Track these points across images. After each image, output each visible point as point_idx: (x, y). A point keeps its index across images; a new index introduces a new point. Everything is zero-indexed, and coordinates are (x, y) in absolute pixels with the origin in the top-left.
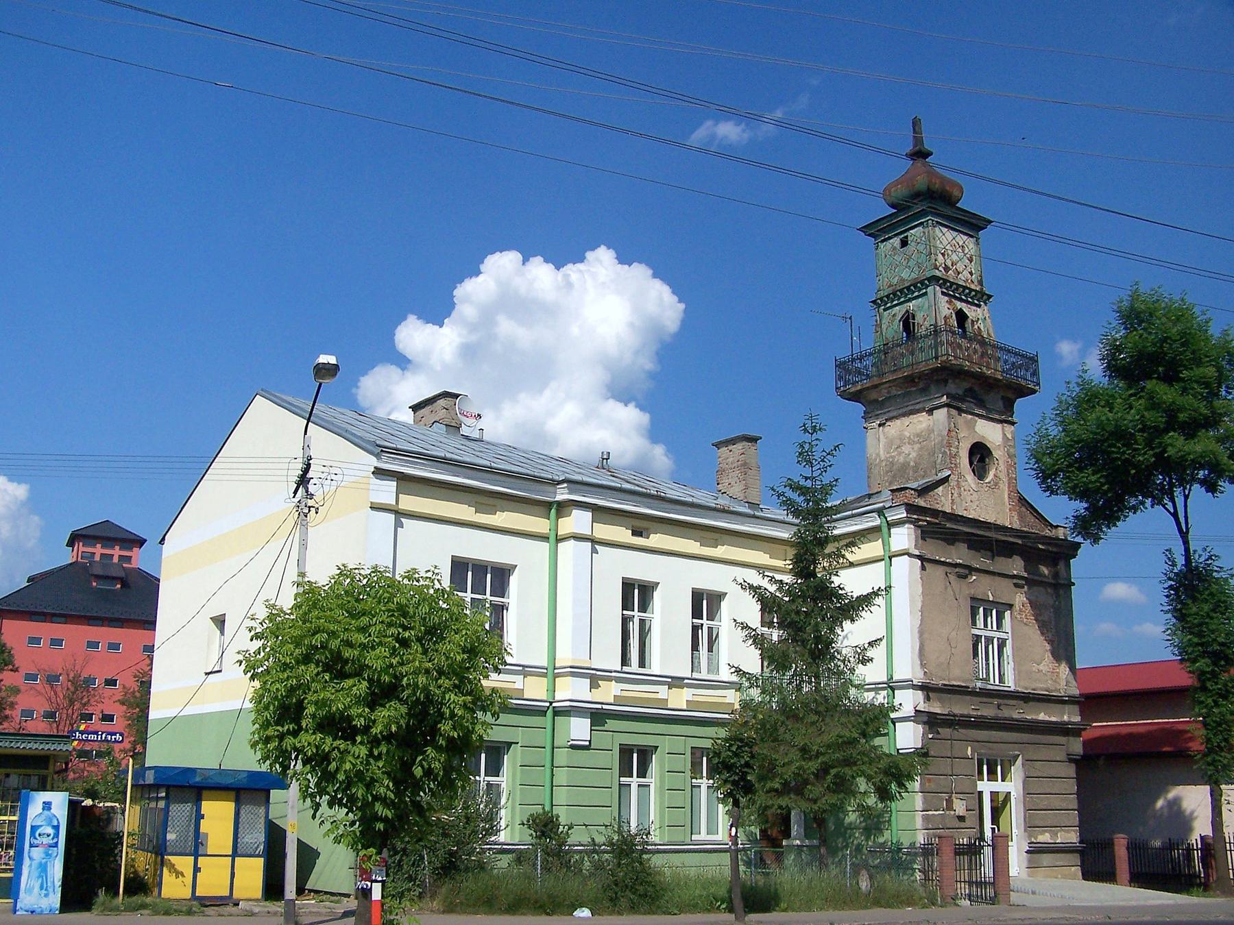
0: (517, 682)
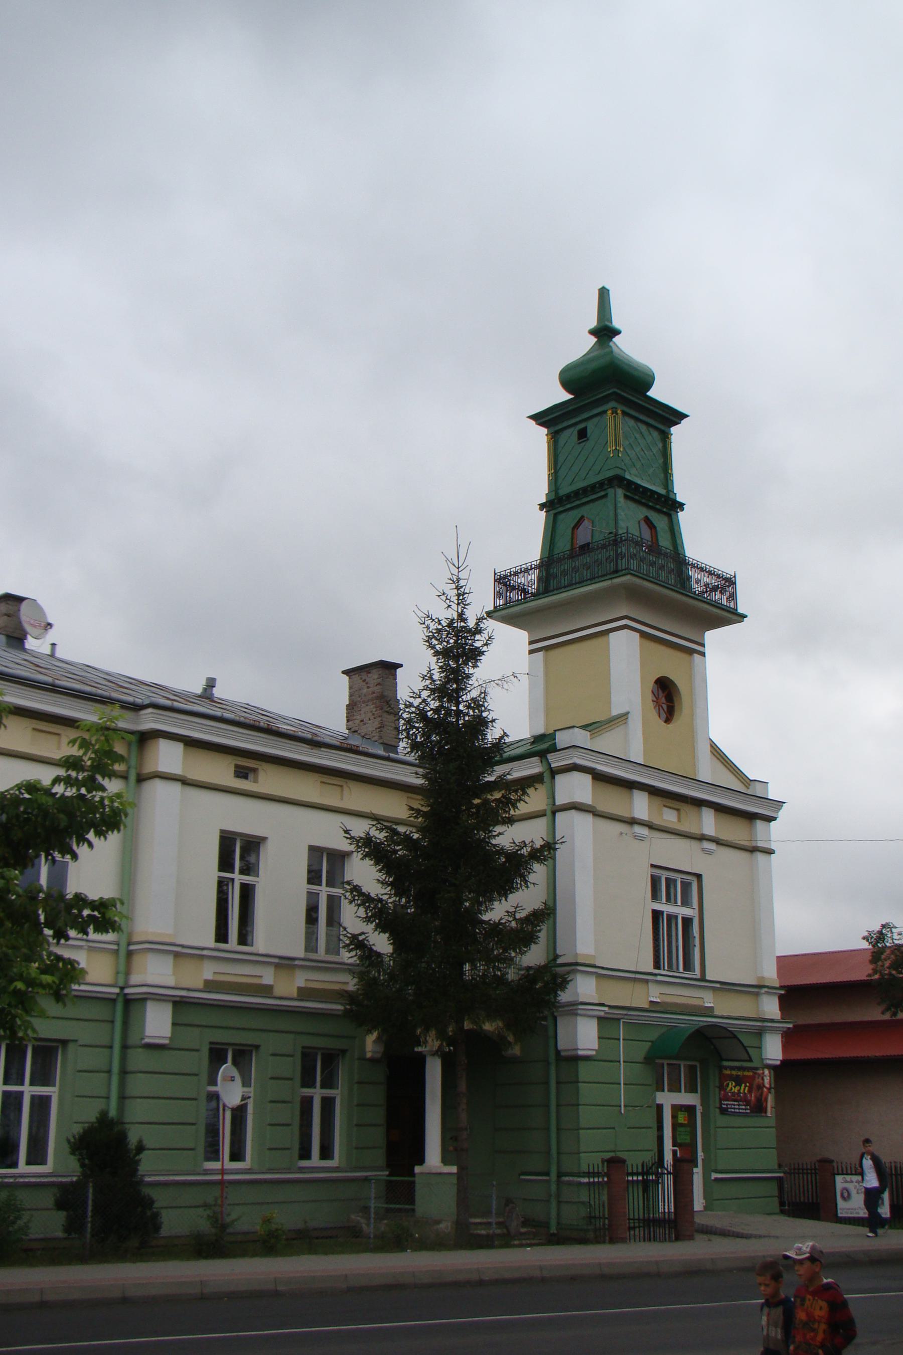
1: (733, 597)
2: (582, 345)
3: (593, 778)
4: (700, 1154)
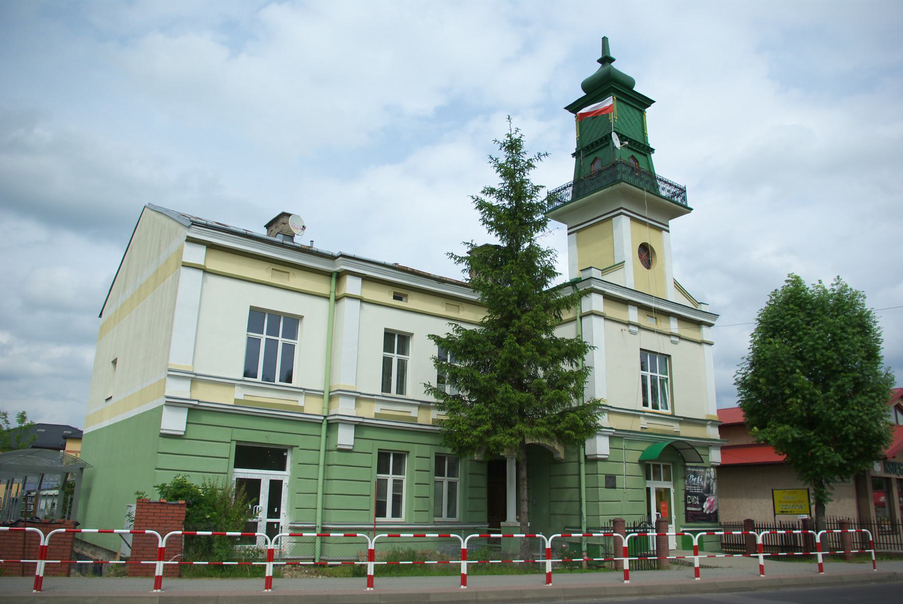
0: (301, 401)
1: (684, 199)
2: (593, 68)
4: (673, 516)
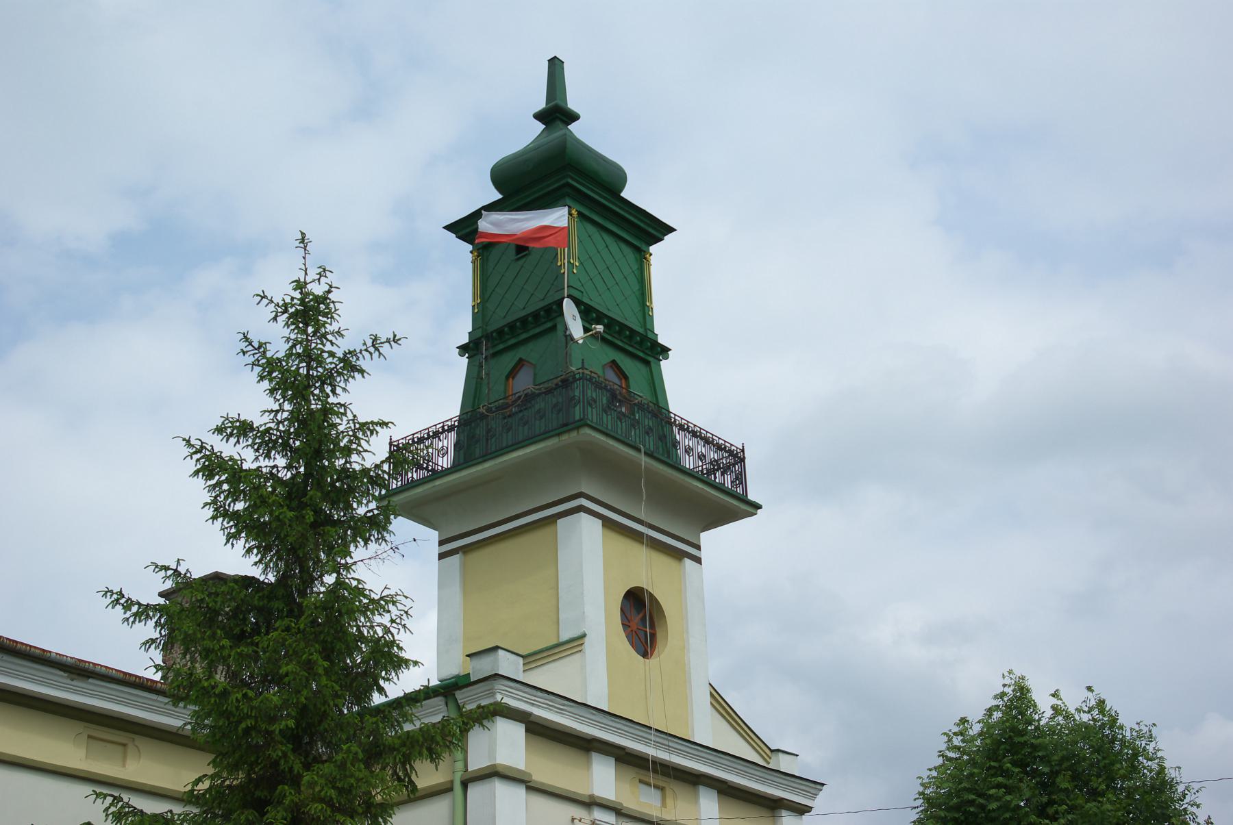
1: (741, 478)
2: (525, 133)
3: (527, 731)
